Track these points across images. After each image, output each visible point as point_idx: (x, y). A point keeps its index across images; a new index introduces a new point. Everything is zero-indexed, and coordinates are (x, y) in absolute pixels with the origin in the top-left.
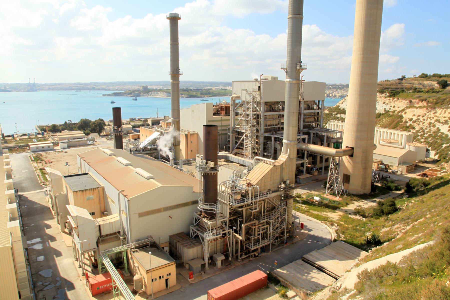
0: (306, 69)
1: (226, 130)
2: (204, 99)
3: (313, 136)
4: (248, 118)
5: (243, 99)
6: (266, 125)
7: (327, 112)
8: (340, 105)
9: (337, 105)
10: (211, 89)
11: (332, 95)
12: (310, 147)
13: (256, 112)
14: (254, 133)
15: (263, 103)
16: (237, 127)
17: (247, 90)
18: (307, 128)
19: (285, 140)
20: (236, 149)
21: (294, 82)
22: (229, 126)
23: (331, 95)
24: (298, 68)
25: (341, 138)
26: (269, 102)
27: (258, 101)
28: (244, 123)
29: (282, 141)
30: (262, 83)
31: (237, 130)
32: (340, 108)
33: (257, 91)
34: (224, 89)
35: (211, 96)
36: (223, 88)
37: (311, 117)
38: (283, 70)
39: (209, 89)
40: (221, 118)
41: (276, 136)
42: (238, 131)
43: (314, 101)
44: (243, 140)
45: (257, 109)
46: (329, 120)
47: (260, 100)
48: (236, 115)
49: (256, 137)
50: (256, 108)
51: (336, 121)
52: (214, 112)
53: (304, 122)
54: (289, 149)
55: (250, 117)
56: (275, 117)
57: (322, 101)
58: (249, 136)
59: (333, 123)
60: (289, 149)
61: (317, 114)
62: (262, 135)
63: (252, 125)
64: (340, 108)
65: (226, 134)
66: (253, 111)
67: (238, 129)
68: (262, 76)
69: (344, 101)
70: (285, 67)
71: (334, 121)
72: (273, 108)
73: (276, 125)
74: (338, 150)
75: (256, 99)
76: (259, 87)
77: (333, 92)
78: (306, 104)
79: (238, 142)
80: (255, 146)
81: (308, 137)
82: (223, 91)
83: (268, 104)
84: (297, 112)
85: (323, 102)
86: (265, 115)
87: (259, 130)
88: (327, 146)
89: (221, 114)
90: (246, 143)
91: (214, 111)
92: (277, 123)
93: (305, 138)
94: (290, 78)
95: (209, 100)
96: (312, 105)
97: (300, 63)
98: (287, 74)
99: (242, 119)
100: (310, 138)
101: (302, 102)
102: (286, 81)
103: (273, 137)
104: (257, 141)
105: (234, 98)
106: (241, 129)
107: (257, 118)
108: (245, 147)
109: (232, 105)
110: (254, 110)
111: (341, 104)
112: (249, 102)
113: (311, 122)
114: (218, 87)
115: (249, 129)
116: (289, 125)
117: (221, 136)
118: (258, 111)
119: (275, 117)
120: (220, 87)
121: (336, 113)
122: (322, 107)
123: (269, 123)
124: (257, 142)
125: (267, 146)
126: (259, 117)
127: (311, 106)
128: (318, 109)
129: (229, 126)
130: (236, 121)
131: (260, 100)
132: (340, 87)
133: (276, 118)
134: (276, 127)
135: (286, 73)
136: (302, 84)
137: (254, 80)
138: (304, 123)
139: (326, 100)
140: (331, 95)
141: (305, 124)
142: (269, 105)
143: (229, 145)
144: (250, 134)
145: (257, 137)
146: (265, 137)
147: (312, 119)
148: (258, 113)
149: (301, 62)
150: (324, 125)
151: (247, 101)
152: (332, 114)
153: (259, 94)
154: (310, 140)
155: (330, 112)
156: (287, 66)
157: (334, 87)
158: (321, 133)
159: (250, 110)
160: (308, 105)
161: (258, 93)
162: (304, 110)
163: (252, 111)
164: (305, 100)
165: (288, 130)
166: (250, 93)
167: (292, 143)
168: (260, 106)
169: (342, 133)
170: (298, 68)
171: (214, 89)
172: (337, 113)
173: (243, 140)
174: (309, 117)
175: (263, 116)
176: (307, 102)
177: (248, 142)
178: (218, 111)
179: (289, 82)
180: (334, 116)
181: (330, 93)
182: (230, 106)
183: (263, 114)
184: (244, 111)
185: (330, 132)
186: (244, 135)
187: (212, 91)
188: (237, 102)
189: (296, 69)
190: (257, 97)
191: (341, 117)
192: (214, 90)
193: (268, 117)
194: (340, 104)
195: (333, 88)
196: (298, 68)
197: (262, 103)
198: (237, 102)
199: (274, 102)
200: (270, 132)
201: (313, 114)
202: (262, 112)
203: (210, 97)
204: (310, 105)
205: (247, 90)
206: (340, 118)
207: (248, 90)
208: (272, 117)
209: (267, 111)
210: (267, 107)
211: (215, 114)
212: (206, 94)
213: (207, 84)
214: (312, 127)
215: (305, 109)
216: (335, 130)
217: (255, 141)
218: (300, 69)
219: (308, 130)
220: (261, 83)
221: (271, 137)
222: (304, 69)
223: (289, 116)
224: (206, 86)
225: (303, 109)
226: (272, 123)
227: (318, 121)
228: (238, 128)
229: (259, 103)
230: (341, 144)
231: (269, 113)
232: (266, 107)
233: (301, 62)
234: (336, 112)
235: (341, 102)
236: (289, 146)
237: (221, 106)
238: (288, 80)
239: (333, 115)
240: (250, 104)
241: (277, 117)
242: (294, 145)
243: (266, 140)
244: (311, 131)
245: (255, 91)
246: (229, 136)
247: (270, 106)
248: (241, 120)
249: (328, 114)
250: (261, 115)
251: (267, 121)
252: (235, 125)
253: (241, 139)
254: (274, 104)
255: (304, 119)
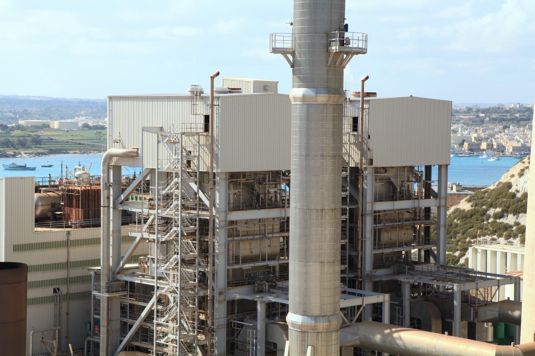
0: (362, 51)
1: (86, 279)
2: (19, 161)
3: (414, 298)
4: (166, 231)
5: (149, 163)
6: (236, 259)
7: (465, 206)
8: (513, 181)
9: (504, 179)
10: (46, 126)
11: (490, 146)
12: (400, 338)
13: (195, 212)
14: (192, 289)
15: (224, 176)
16: (127, 266)
17: (161, 129)
18: (389, 266)
19: (296, 313)
20: (124, 352)
21: (322, 98)
22: (97, 262)
23: (484, 146)
24: (335, 48)
25: (517, 303)
26: (244, 174)
27: (203, 169)
28: (155, 252)
29: (284, 314)
30: (215, 103)
31: (129, 279)
32: (512, 190)
33: (198, 134)
34: (95, 128)
35: (43, 154)
36: (90, 124)
37: (401, 227)
38: (280, 56)
39: (37, 128)
40: (68, 233)
41: (272, 299)
42: (132, 284)
43: (412, 168)
44: (150, 317)
45: (200, 200)
46: (475, 237)
47: (212, 168)
48: (123, 224)
49: (200, 303)
50: (196, 194)
51: (502, 240)
52: (38, 212)
53: (377, 243)
54: (309, 349)
55: (175, 229)
56: (269, 228)
57: (440, 167)
58: (172, 299)
59: (490, 248)
60: (309, 349)
61: (423, 214)
62: (222, 297)
63: (183, 260)
64: (512, 190)
65: (87, 295)
66: (185, 207)
67: (133, 274)
68: (215, 79)
69: (526, 165)
70: (288, 45)
71: (494, 240)
72: (262, 196)
73: (272, 257)
74: (503, 348)
75: (195, 161)
76: (207, 118)
77: (492, 136)
78: (381, 179)
79: (131, 326)
80: (195, 337)
81: (391, 299)
82: (92, 134)
83: (243, 180)
84: (334, 210)
85: (443, 170)
86: (232, 223)
87: (210, 276)
88: (466, 332)
89: (69, 218)
90: (159, 328)
91: (40, 209)
92: (278, 250)
93: (381, 304)
94: (307, 87)
95: (39, 168)
96: (402, 182)
97: (340, 30)
98: (294, 73)
99: (146, 235)
100: (401, 305)
101: (368, 173)
102: (291, 96)
103: (262, 302)
104: (202, 317)
105: (115, 159)
106: (143, 276)
107: (201, 234)
108: (158, 345)
109: (108, 187)
110: (190, 203)
111: (517, 176)
112: (171, 173)
113: (401, 245)
114: (71, 117)
115: (171, 273)
116: (306, 259)
117: (64, 305)
118: (202, 206)
119: (269, 228)
120: (81, 121)
121: (499, 210)
122: (439, 189)
123: (245, 250)
124: (203, 322)
125: (240, 338)
126: (207, 230)
127: (402, 186)
128: (427, 196)
129: (99, 265)
130: (123, 246)
131: (212, 168)
132: (518, 115)
133: (273, 233)
134: (271, 263)
135: (292, 66)
136: (366, 106)
137: (189, 94)
138: (374, 249)
139: (455, 162)
140: (484, 146)
141: (380, 251)
142: (244, 184)
143: (95, 339)
144: (174, 292)
145: (202, 303)
146: (231, 304)
147: (406, 235)
148: (204, 213)
149: (346, 27)
150: (457, 254)
151: (165, 168)
152: (484, 213)
153: (206, 145)
154: (402, 313)
155: (476, 205)
156: (294, 40)
157: (494, 116)
158: (441, 284)
159: (175, 203)
160: (390, 183)
161: (203, 140)
162: (375, 200)
163: (183, 205)
164: (375, 164)
165: (305, 277)
166: (172, 140)
167: (322, 325)
168: (213, 189)
169: (517, 281)
170: (334, 48)
171: (56, 124)
172: (503, 211)
173: (150, 317)
174: (393, 228)
175: (223, 224)
176: (386, 172)
177: (170, 324)
178: (55, 206)
179: (304, 98)
180: (491, 220)
181: (479, 140)
182: (101, 188)
183: (223, 218)
184: (152, 207)
185: (473, 279)
186: (154, 299)
187: (48, 133)
188: (127, 172)
189: (328, 52)
190: (199, 157)
191: (517, 224)
192: (56, 130)
193: (241, 228)
194: (513, 176)
195: (494, 120)
196: (334, 48)
197: (217, 178)
198: (127, 172)
199: (265, 173)
200: (249, 284)
201: (407, 216)
202: (218, 211)
203: (38, 154)
204: (397, 183)
205: (161, 129)
206: (514, 228)
207: (165, 128)
208: (257, 228)
209: (237, 208)
210: (236, 191)
211: (40, 221)
212: (23, 144)
213: (29, 109)
214: (407, 264)
215: (379, 198)
216: (498, 273)
217: (193, 320)
218: (340, 53)
219: (394, 274)
220: (212, 105)
221: (255, 303)
222: (357, 53)
223: (305, 225)
224: (26, 114)
225: (369, 197)
226: (256, 251)
227: (427, 239)
228: (132, 272)
229: (206, 175)
230: (517, 327)
231: (244, 212)
232: (232, 191)
233: (346, 27)
234: (500, 206)
235: (518, 171)
236: (311, 337)
237: (69, 191)
238: (300, 92)
239: (488, 220)
240: (175, 180)
241: (277, 227)
242: (329, 332)
243: (235, 316)
244: (401, 278)
245: (192, 134)
246: (97, 302)
247: (250, 187)
248: (142, 239)
249: (472, 216)
250: (214, 221)
251: (238, 242)
252: (118, 258)
253: (143, 314)
254: (264, 180)
255: (377, 233)
